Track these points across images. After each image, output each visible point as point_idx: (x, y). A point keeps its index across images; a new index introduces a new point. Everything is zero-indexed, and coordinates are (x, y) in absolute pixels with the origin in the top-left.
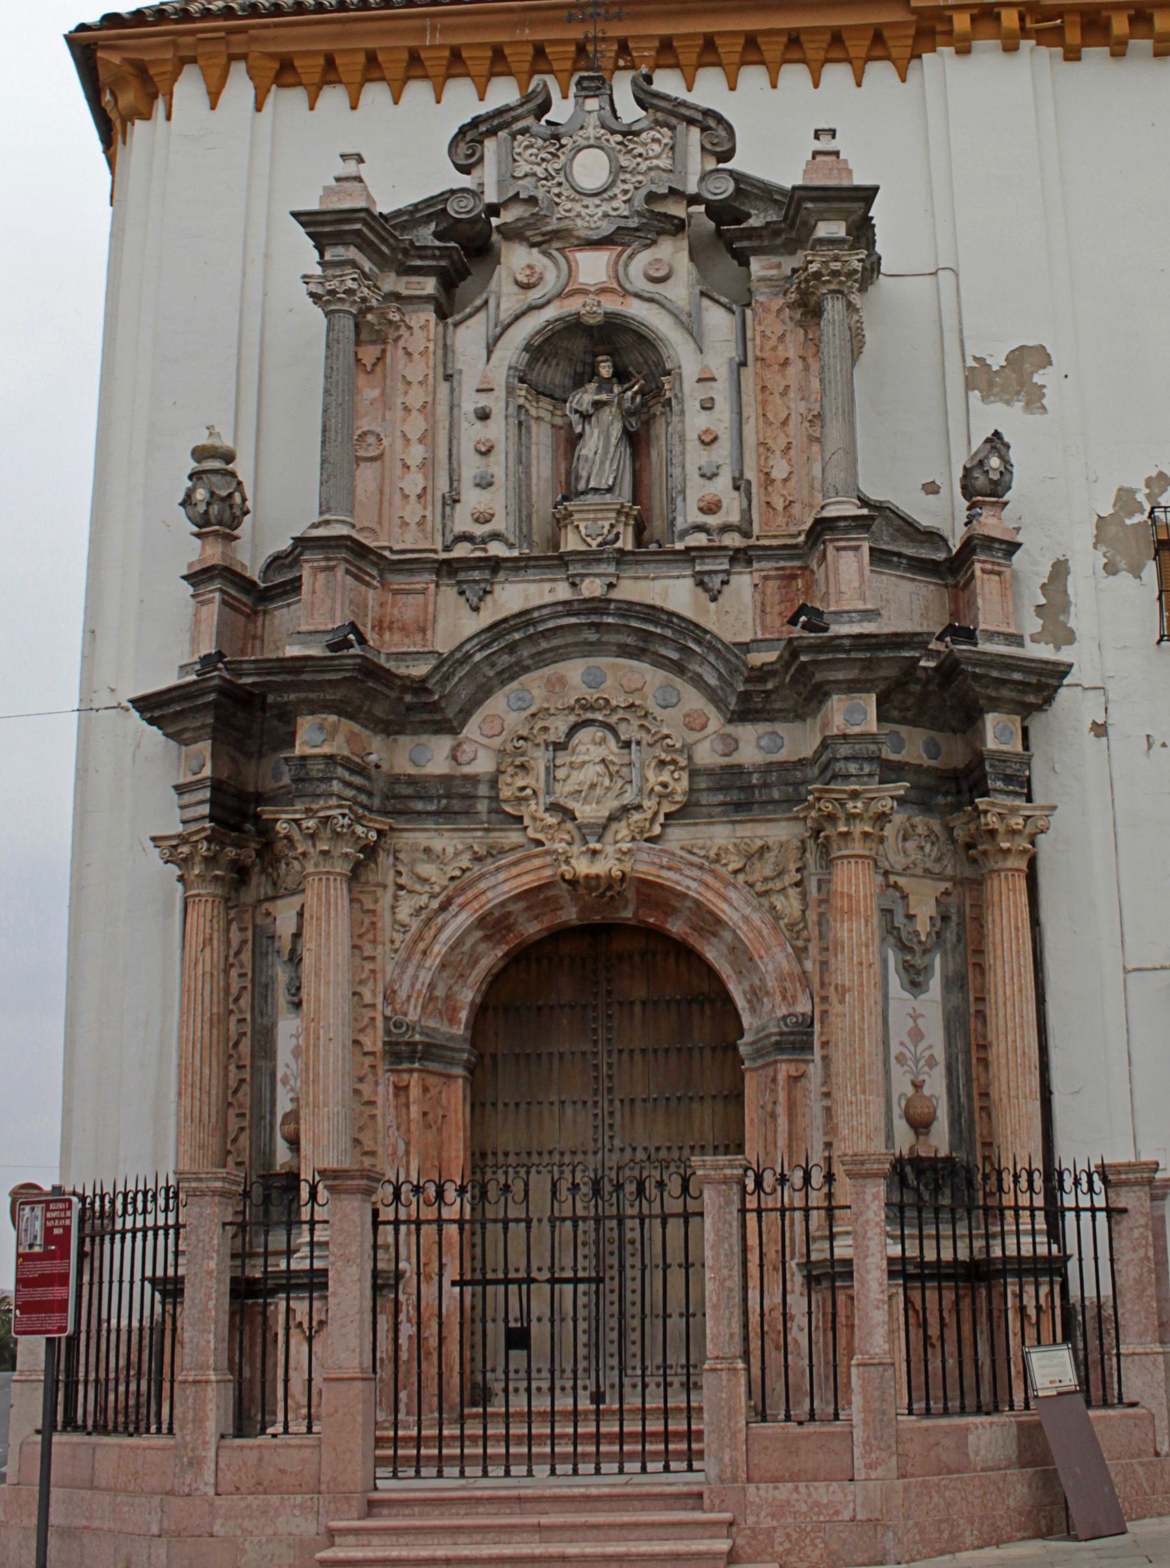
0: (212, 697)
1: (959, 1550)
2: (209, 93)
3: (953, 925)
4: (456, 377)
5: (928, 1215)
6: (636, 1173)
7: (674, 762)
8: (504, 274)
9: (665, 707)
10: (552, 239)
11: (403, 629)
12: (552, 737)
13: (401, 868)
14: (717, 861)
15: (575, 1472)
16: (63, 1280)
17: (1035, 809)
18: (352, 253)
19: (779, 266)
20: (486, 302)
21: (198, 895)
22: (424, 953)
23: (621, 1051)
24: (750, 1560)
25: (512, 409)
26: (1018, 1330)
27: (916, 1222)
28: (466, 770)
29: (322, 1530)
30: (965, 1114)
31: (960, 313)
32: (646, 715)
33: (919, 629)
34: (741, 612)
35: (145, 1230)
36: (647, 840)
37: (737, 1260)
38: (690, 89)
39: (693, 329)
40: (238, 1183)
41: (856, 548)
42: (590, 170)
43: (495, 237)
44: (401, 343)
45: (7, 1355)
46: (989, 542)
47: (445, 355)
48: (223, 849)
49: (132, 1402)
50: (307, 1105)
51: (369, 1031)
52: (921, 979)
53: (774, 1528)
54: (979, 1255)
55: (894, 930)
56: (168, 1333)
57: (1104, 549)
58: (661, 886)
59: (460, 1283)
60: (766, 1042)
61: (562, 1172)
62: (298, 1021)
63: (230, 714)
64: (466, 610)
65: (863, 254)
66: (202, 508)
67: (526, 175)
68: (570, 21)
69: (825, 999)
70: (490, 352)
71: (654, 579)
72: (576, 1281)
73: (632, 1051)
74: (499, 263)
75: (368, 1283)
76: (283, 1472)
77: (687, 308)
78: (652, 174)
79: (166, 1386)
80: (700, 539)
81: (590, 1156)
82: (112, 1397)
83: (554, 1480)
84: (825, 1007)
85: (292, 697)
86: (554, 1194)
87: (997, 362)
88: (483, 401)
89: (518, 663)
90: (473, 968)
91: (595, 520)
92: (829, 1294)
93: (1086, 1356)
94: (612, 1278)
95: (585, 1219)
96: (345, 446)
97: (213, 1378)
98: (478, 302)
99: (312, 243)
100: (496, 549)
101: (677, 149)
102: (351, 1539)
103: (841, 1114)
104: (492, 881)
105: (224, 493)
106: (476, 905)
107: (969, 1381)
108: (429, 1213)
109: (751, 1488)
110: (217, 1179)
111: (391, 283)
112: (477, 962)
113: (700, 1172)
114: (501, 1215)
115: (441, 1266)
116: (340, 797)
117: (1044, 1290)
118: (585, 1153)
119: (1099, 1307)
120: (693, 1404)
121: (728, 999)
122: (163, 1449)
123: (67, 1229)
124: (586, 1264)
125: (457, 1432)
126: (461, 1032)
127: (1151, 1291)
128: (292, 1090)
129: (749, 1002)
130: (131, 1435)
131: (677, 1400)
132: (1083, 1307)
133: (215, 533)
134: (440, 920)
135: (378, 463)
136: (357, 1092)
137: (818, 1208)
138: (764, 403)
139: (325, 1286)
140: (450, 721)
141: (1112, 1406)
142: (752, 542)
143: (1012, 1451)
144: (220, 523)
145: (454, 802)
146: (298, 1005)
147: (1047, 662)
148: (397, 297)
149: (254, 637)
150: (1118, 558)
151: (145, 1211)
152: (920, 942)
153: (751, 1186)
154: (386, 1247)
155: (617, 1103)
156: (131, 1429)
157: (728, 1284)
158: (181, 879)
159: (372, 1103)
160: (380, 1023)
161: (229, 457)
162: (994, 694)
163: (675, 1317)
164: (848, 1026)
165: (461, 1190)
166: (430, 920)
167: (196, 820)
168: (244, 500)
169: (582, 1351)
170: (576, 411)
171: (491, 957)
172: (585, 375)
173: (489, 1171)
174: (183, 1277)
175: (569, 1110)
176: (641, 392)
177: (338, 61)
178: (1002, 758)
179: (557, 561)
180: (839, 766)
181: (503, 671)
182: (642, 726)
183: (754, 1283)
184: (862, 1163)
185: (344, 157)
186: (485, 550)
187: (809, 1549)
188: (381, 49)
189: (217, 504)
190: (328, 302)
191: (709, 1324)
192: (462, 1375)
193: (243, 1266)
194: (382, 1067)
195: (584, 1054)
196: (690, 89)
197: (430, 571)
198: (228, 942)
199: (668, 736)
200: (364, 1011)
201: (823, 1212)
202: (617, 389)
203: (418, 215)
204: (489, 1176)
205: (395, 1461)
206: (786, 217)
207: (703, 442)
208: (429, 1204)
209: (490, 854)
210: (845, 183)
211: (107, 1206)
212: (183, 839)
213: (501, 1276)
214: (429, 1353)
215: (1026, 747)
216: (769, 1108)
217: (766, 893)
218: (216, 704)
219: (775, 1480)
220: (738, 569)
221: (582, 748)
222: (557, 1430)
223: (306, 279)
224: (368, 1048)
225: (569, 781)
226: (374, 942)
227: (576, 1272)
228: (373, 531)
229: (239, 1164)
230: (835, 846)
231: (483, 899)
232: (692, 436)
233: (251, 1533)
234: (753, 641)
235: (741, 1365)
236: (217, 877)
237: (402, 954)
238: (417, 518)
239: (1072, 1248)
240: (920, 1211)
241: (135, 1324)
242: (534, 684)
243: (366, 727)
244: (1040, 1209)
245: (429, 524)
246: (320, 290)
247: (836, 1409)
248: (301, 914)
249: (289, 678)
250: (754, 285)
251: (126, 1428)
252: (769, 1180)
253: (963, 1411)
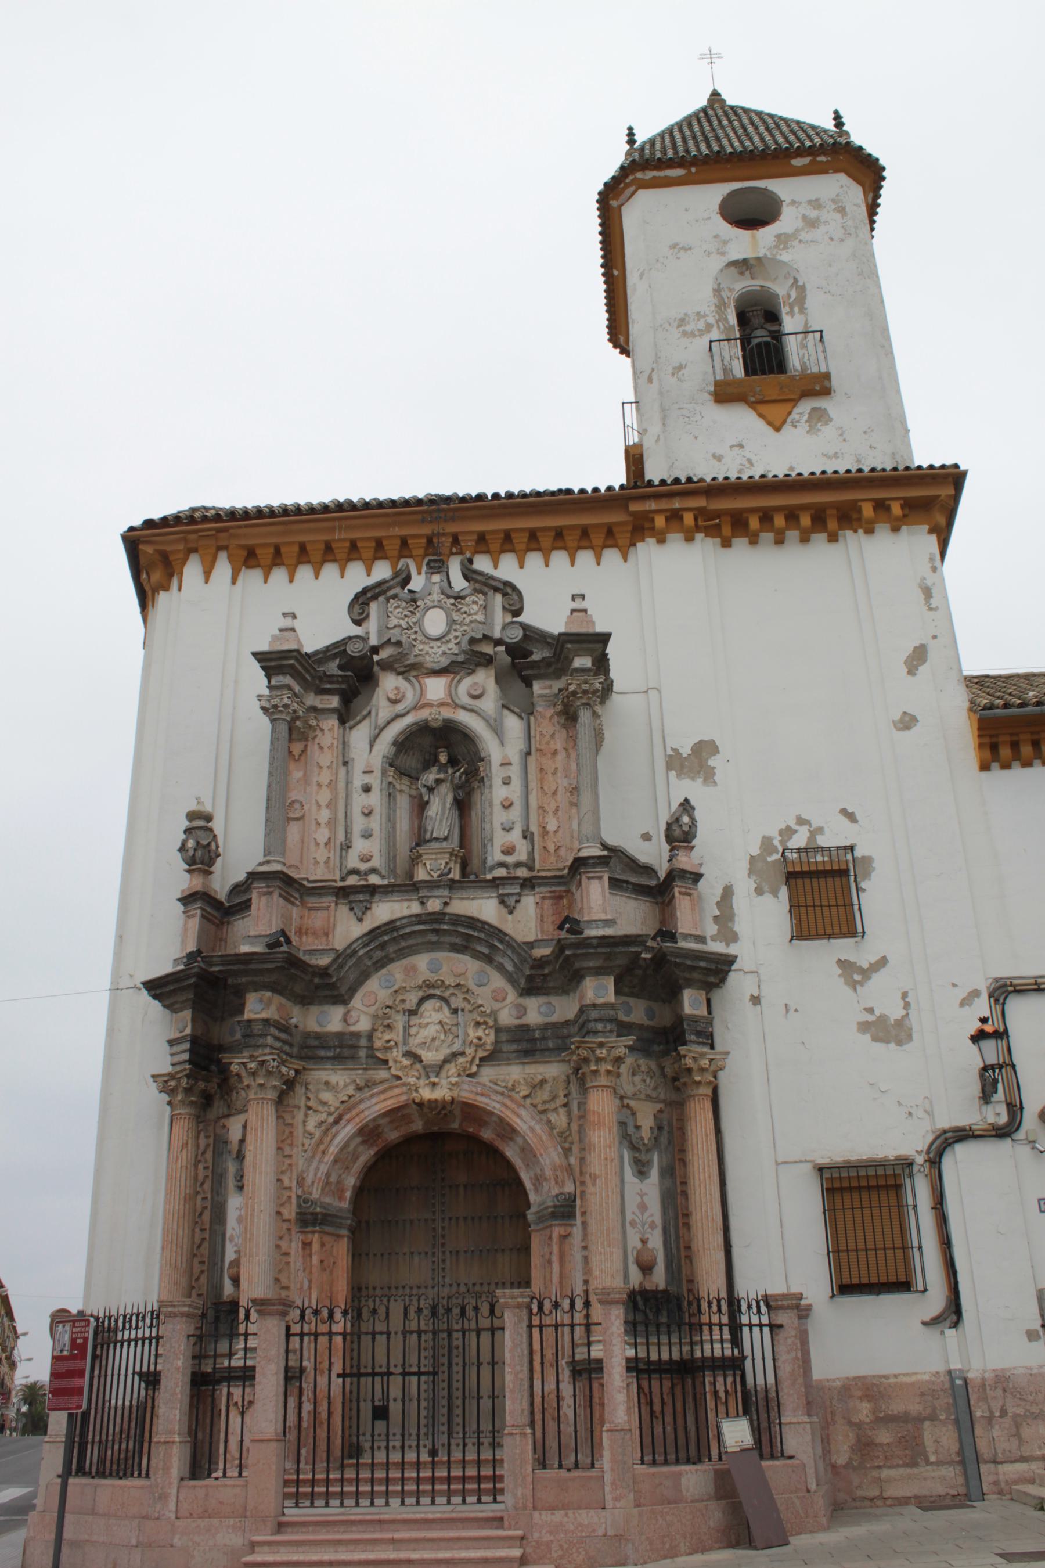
0: (193, 980)
1: (677, 1556)
2: (205, 572)
3: (665, 1133)
4: (350, 763)
5: (652, 1329)
6: (460, 1301)
7: (485, 1023)
8: (381, 693)
9: (479, 986)
10: (410, 669)
11: (314, 933)
12: (407, 1006)
13: (310, 1095)
14: (513, 1090)
15: (418, 1503)
16: (81, 1373)
17: (716, 1054)
18: (288, 680)
19: (550, 687)
20: (370, 713)
21: (180, 1114)
22: (324, 1152)
23: (450, 1219)
24: (535, 1563)
25: (385, 785)
26: (713, 1407)
27: (644, 1334)
28: (353, 1029)
29: (247, 1542)
30: (675, 1261)
31: (662, 719)
32: (468, 991)
33: (640, 932)
34: (528, 921)
35: (136, 1340)
36: (468, 1076)
37: (526, 1360)
38: (496, 568)
39: (497, 729)
40: (199, 1309)
41: (600, 878)
42: (435, 622)
43: (376, 668)
44: (317, 741)
45: (42, 1424)
46: (683, 874)
47: (344, 748)
48: (196, 1083)
49: (122, 1456)
50: (245, 1255)
51: (287, 1205)
52: (645, 1169)
53: (552, 1541)
54: (686, 1356)
55: (627, 1137)
56: (149, 1410)
57: (754, 878)
58: (477, 1107)
59: (343, 1375)
60: (545, 1212)
61: (411, 1300)
62: (240, 1199)
64: (354, 921)
65: (602, 679)
66: (191, 853)
67: (395, 627)
68: (423, 522)
69: (583, 1183)
70: (372, 746)
71: (473, 899)
72: (419, 1374)
73: (458, 1219)
74: (377, 685)
75: (282, 1376)
76: (221, 1503)
77: (494, 716)
78: (473, 625)
79: (146, 1445)
80: (501, 872)
81: (430, 1290)
82: (109, 1452)
83: (403, 1508)
84: (583, 1188)
85: (244, 980)
86: (406, 1315)
87: (686, 751)
88: (367, 779)
89: (386, 957)
90: (355, 1162)
91: (436, 859)
92: (587, 1383)
93: (759, 1425)
94: (443, 1372)
95: (426, 1332)
96: (281, 812)
97: (177, 1440)
98: (365, 712)
99: (263, 673)
100: (374, 880)
101: (488, 608)
102: (266, 1549)
103: (595, 1260)
104: (368, 1104)
105: (205, 843)
106: (357, 1120)
107: (681, 1441)
108: (323, 1328)
109: (536, 1514)
110: (185, 1305)
111: (312, 700)
112: (357, 1158)
113: (502, 1300)
114: (371, 1330)
115: (331, 1364)
116: (272, 1047)
117: (730, 1380)
118: (426, 1287)
119: (767, 1391)
120: (497, 1457)
121: (520, 1183)
122: (142, 1488)
123: (86, 1339)
124: (426, 1362)
125: (339, 1476)
126: (346, 1206)
127: (800, 1380)
128: (236, 1245)
129: (534, 1185)
130: (121, 1478)
131: (486, 1455)
132: (756, 1391)
133: (199, 870)
134: (334, 1130)
135: (301, 822)
136: (278, 1247)
137: (580, 1324)
138: (542, 780)
139: (253, 1377)
140: (342, 996)
141: (777, 1458)
142: (535, 874)
143: (711, 1489)
144: (202, 863)
145: (345, 1050)
146: (241, 1188)
147: (721, 955)
148: (314, 709)
149: (221, 940)
150: (764, 884)
151: (137, 1327)
152: (644, 1144)
153: (535, 1309)
154: (295, 1351)
155: (448, 1253)
156: (121, 1474)
157: (520, 1376)
158: (169, 1103)
159: (287, 1254)
160: (294, 1200)
161: (209, 818)
162: (688, 976)
163: (485, 1398)
164: (599, 1201)
165: (345, 1313)
166: (327, 1130)
167: (180, 1063)
168: (217, 847)
169: (423, 1421)
170: (425, 786)
171: (366, 1155)
173: (363, 1299)
174: (160, 1372)
175: (416, 1259)
176: (466, 773)
177: (283, 550)
178: (695, 1019)
179: (410, 887)
180: (591, 1025)
181: (377, 962)
182: (465, 999)
183: (537, 1375)
184: (609, 1294)
185: (285, 615)
186: (367, 880)
187: (575, 1555)
188: (309, 541)
189: (200, 849)
190: (273, 713)
191: (508, 1403)
192: (343, 1438)
193: (200, 1364)
195: (426, 1220)
196: (496, 568)
197: (332, 894)
198: (198, 1146)
199: (481, 1006)
200: (284, 1191)
201: (583, 1327)
202: (450, 771)
204: (363, 1303)
205: (297, 1496)
206: (555, 654)
207: (504, 806)
208: (324, 1322)
209: (367, 1086)
210: (591, 631)
211: (113, 1323)
212: (172, 1076)
213: (370, 1370)
214: (322, 1423)
215: (710, 1012)
216: (547, 1257)
217: (544, 1112)
218: (196, 986)
219: (553, 1508)
220: (526, 892)
221: (427, 1014)
222: (406, 1475)
223: (260, 697)
224: (286, 1216)
225: (419, 1036)
226: (291, 1145)
227: (419, 1368)
228: (297, 868)
229: (199, 1295)
230: (588, 1079)
231: (362, 1116)
233: (199, 1544)
234: (536, 941)
235: (529, 1431)
236: (192, 1102)
237: (310, 1153)
238: (325, 859)
239: (747, 1351)
240: (647, 1326)
241: (127, 1403)
242: (396, 971)
243: (289, 1000)
244: (725, 1325)
245: (332, 863)
246: (267, 705)
247: (593, 1461)
248: (245, 1127)
249: (242, 967)
250: (535, 700)
251: (118, 1474)
252: (547, 1305)
253: (677, 1462)
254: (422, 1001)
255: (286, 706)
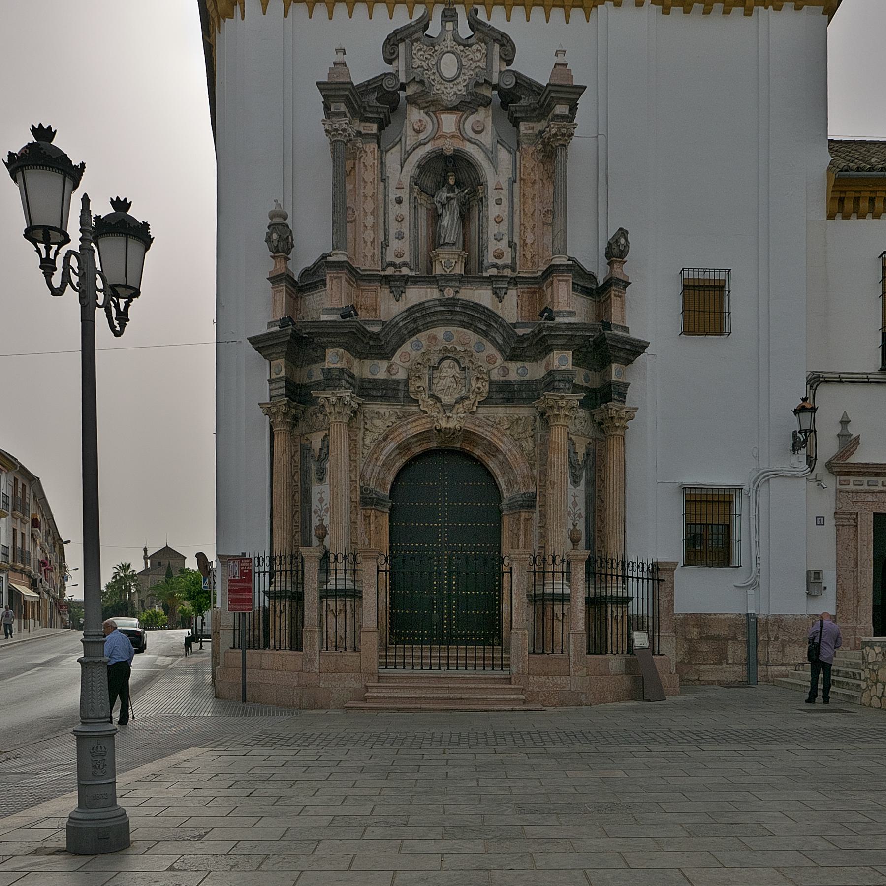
0: (289, 338)
7: (483, 378)
10: (433, 106)
19: (533, 129)
28: (394, 377)
34: (510, 308)
39: (493, 160)
41: (567, 281)
47: (382, 168)
63: (292, 344)
78: (477, 70)
80: (493, 271)
96: (342, 215)
100: (405, 271)
109: (531, 677)
148: (359, 133)
172: (442, 183)
179: (428, 279)
189: (281, 240)
194: (359, 508)
203: (370, 87)
218: (289, 341)
221: (444, 370)
232: (491, 218)
238: (371, 254)
254: (443, 359)
255: (344, 130)
